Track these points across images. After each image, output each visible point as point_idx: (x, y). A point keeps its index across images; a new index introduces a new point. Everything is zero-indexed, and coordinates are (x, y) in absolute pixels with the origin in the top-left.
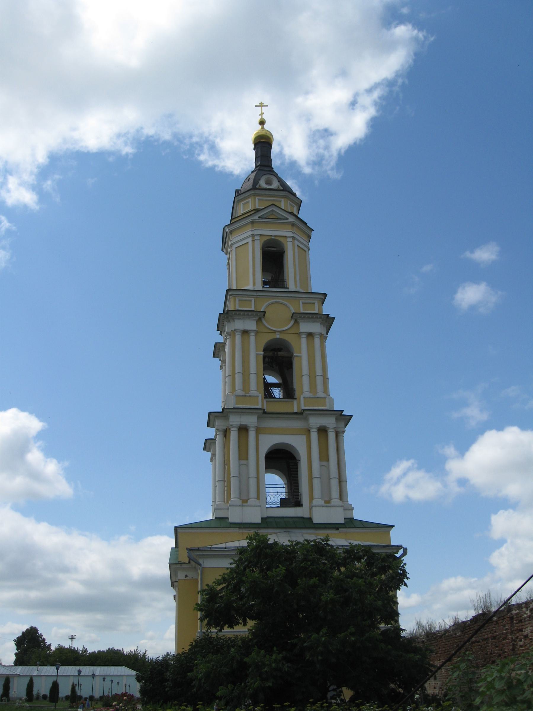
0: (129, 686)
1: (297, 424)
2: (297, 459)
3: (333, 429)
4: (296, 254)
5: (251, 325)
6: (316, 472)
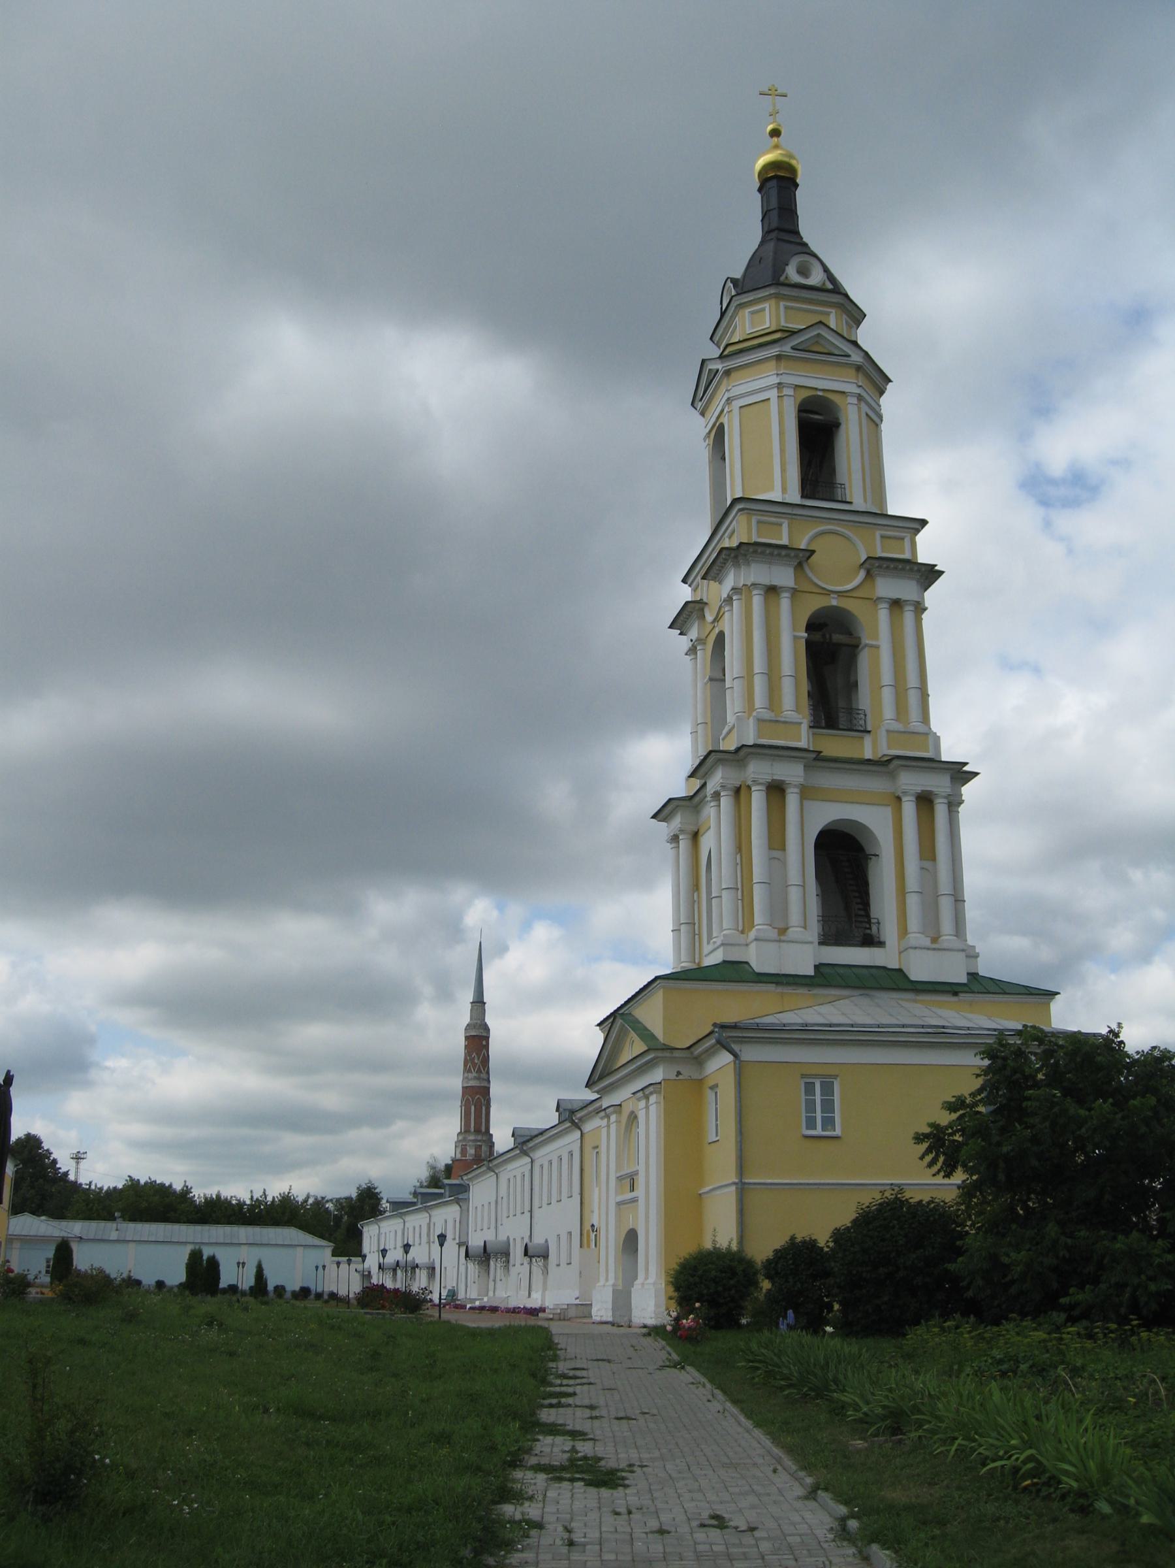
0: (324, 1267)
1: (875, 784)
2: (869, 850)
3: (945, 797)
4: (865, 430)
5: (783, 576)
6: (912, 882)
